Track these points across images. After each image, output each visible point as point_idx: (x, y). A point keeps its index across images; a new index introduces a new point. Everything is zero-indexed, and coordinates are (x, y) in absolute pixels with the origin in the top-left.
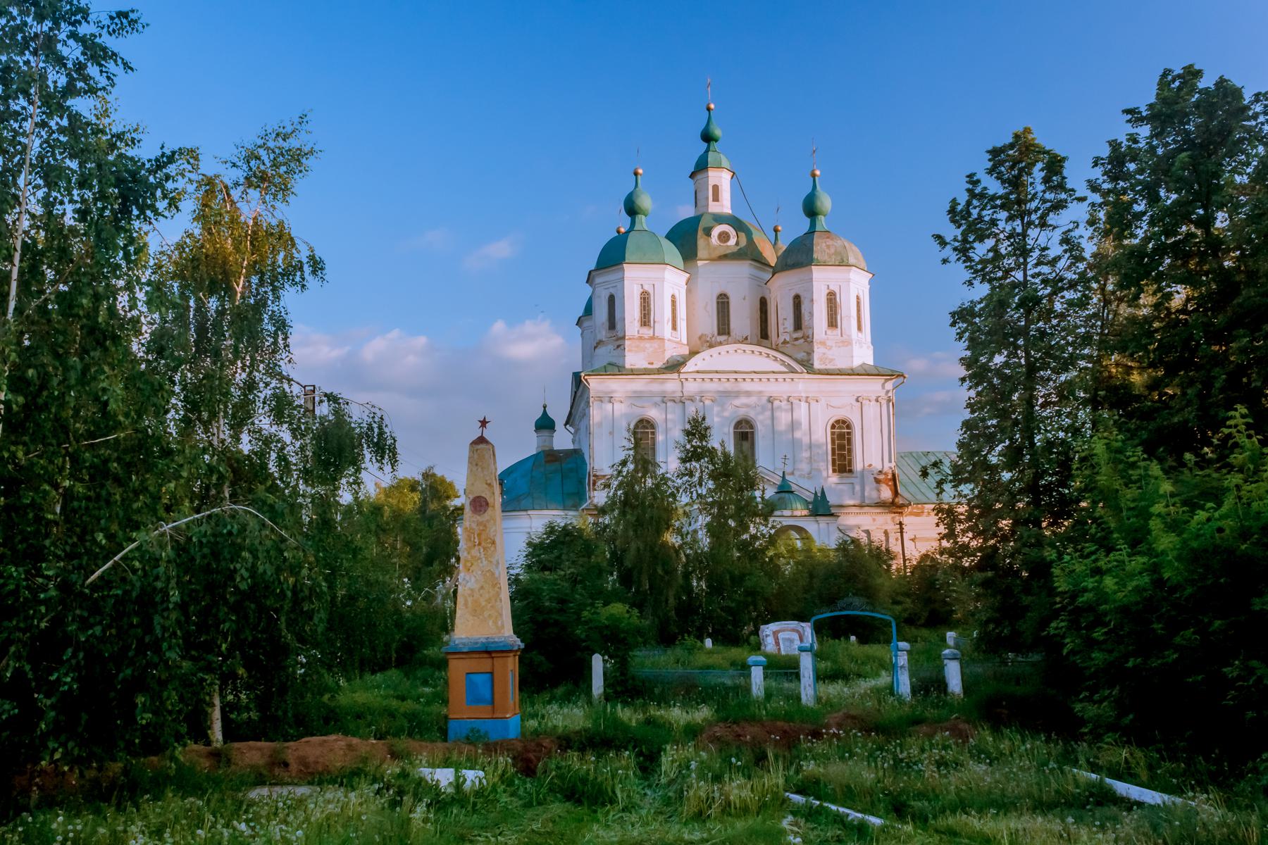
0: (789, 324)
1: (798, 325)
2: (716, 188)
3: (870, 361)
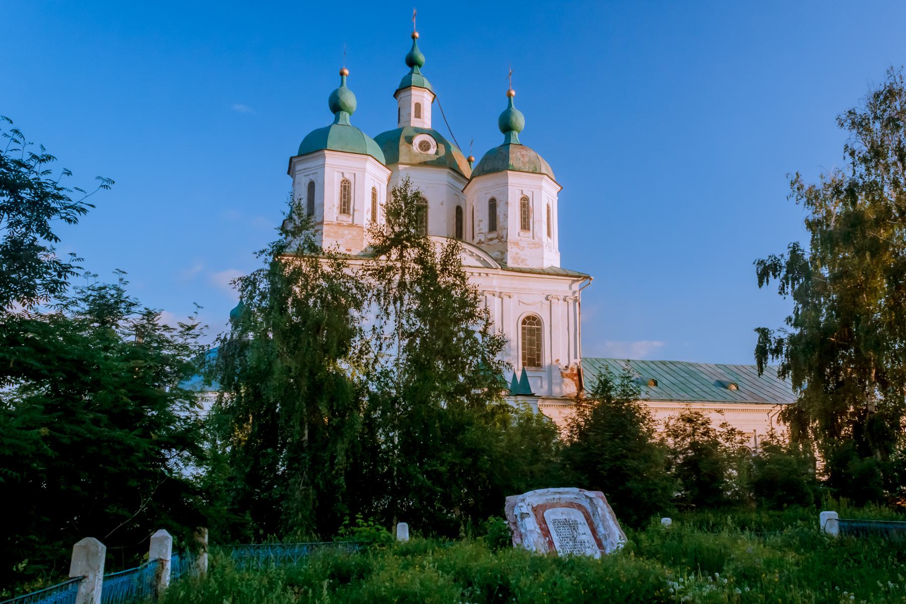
0: (485, 226)
1: (493, 226)
2: (418, 106)
3: (557, 264)
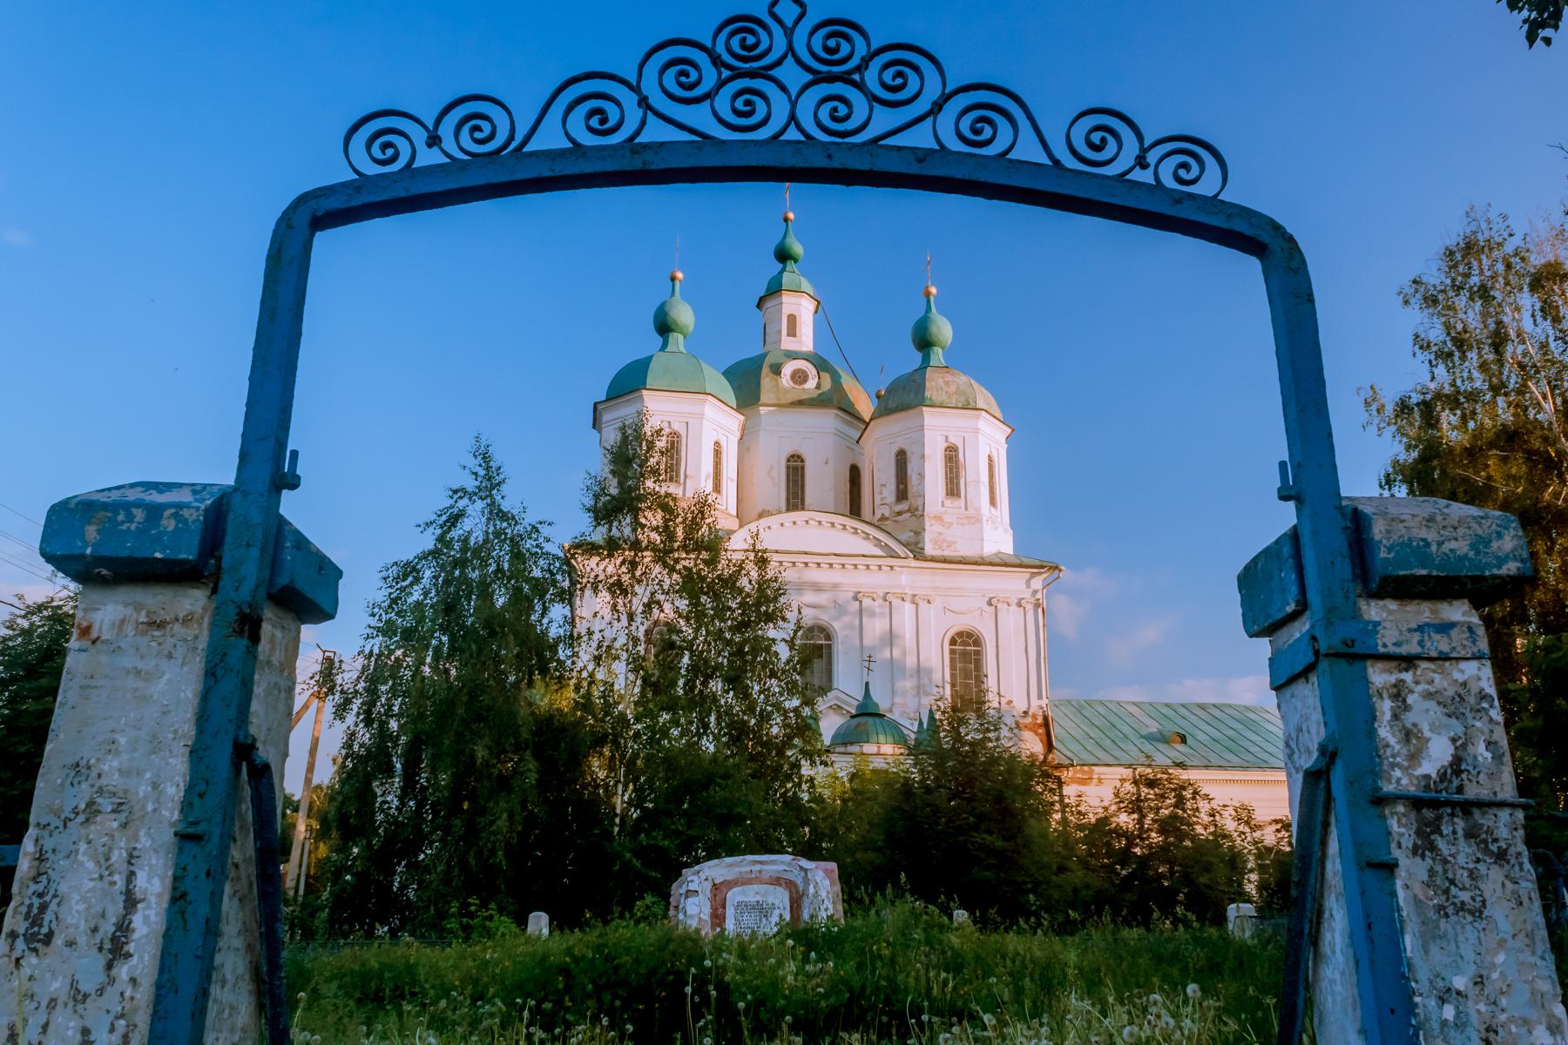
0: (889, 493)
1: (902, 495)
2: (792, 319)
